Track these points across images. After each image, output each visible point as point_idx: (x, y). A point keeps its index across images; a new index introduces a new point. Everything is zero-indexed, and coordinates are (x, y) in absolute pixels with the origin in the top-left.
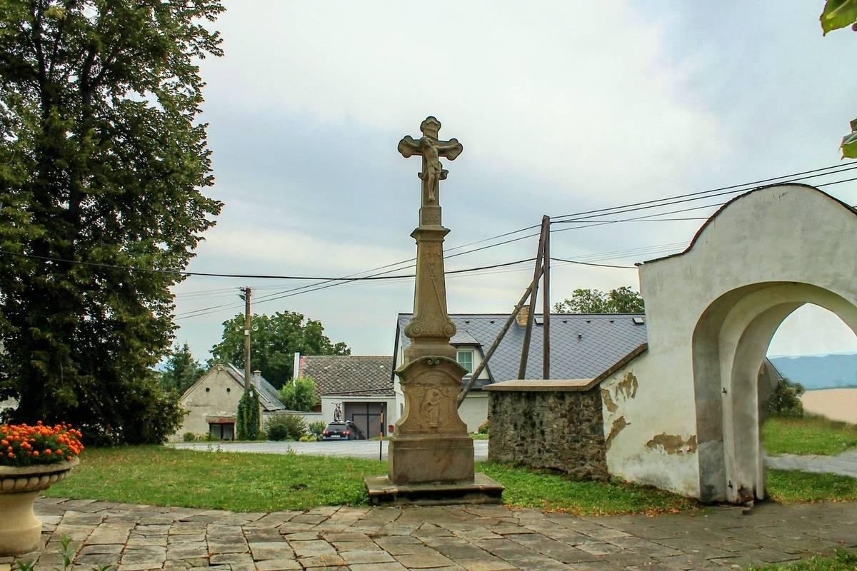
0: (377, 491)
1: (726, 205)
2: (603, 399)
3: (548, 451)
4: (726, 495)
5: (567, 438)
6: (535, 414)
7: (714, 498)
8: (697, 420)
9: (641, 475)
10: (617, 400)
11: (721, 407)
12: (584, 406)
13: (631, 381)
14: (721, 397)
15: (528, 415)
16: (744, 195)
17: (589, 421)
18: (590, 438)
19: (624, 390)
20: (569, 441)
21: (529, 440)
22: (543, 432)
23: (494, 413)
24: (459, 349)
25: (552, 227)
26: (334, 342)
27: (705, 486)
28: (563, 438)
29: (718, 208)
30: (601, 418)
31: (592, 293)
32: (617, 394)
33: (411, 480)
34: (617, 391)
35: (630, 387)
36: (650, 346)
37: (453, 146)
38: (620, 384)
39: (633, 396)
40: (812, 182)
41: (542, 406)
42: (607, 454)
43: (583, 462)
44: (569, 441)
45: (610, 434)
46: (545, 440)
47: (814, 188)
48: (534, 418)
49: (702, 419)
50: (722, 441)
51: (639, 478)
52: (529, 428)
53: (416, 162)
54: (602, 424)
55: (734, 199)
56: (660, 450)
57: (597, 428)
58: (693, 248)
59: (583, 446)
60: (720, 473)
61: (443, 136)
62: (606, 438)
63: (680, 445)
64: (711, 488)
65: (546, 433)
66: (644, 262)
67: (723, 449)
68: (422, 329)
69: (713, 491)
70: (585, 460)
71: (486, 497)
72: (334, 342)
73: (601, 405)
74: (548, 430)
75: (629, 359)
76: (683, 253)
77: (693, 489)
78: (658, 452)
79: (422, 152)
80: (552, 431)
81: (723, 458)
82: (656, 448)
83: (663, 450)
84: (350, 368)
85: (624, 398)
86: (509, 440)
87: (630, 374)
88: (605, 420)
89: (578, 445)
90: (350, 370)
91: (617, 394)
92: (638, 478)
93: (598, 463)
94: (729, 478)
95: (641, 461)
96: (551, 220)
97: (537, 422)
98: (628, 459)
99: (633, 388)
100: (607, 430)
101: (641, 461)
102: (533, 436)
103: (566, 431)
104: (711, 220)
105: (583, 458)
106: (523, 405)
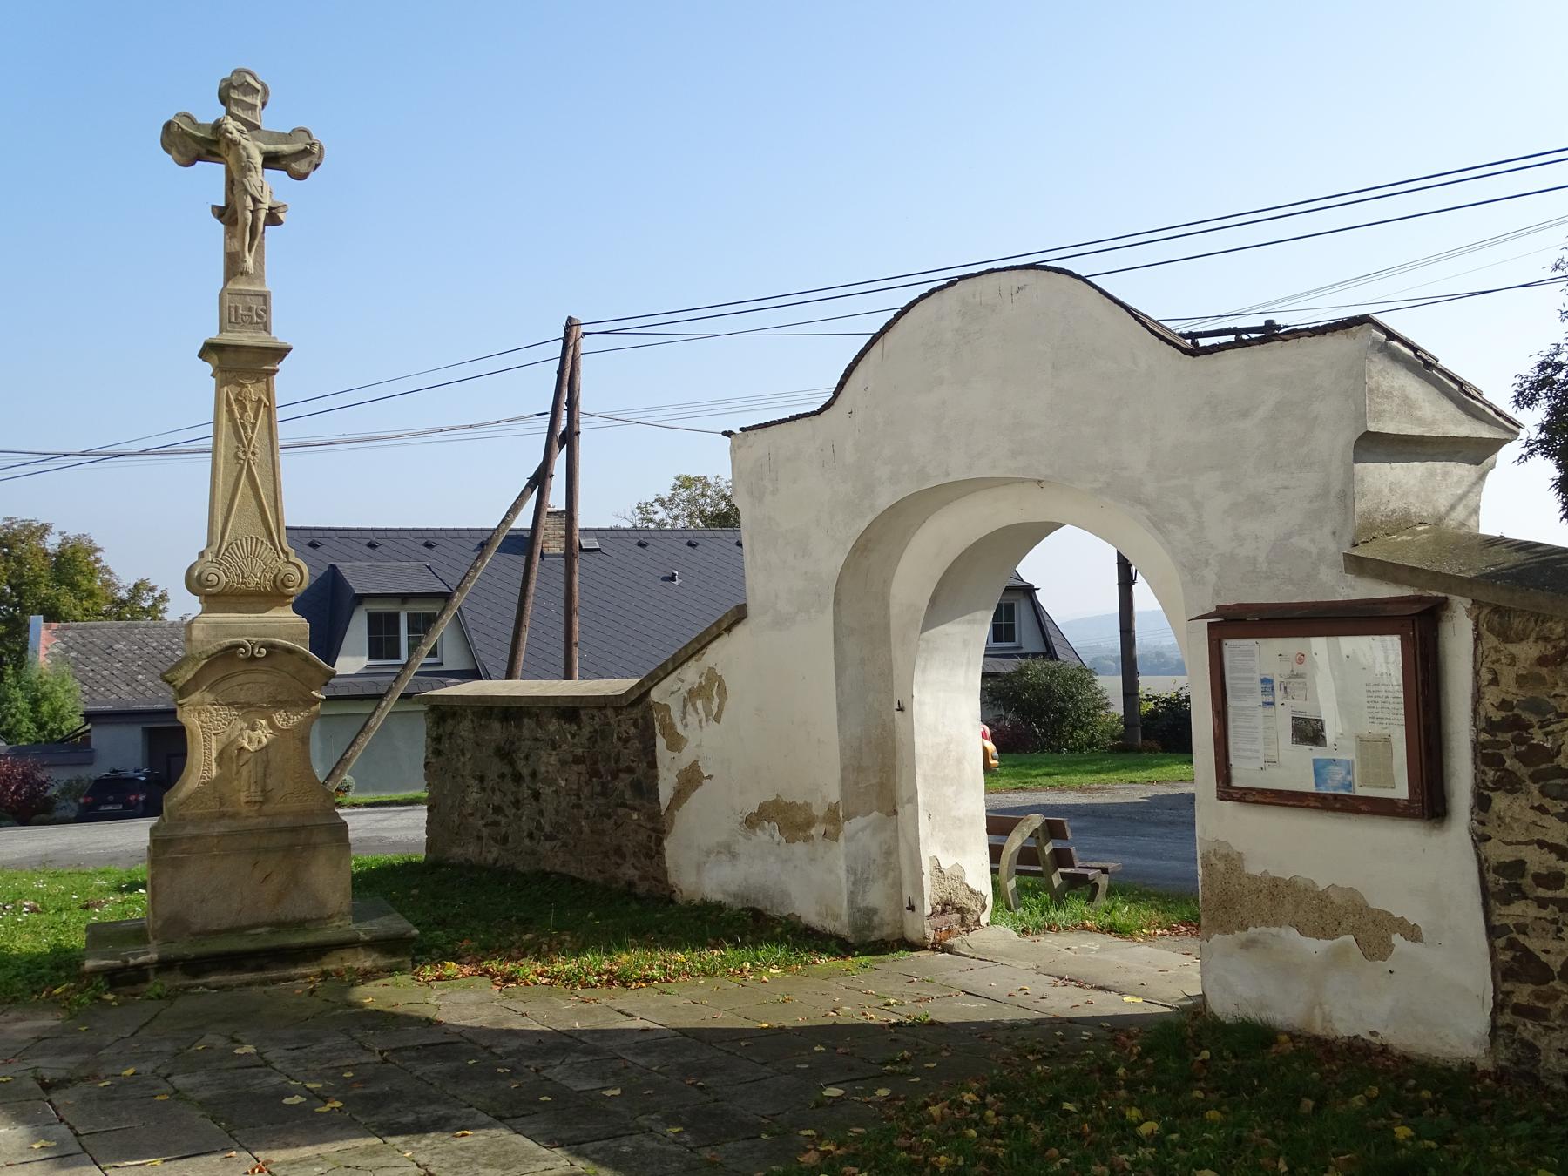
0: (111, 962)
1: (904, 311)
2: (657, 724)
3: (549, 838)
4: (902, 927)
5: (587, 808)
6: (522, 755)
7: (876, 936)
8: (843, 770)
9: (733, 888)
10: (686, 726)
11: (893, 740)
12: (619, 739)
13: (711, 689)
14: (893, 720)
15: (505, 753)
16: (940, 288)
17: (630, 770)
18: (634, 809)
19: (699, 704)
20: (591, 814)
21: (510, 811)
22: (536, 796)
23: (438, 753)
24: (407, 606)
25: (585, 345)
26: (125, 579)
27: (859, 910)
28: (578, 807)
29: (891, 315)
30: (653, 765)
31: (711, 481)
32: (684, 713)
33: (196, 928)
34: (685, 707)
35: (710, 699)
36: (751, 610)
37: (300, 146)
38: (690, 692)
39: (717, 719)
40: (1078, 266)
41: (536, 739)
42: (665, 843)
43: (619, 861)
44: (591, 814)
45: (672, 800)
46: (541, 813)
47: (1084, 279)
48: (521, 764)
49: (852, 768)
50: (896, 812)
51: (729, 895)
52: (509, 785)
53: (210, 178)
54: (656, 777)
55: (923, 297)
56: (768, 834)
57: (646, 788)
58: (836, 403)
59: (617, 825)
60: (890, 880)
61: (274, 119)
62: (664, 808)
63: (810, 823)
64: (870, 912)
65: (543, 797)
66: (742, 429)
67: (896, 830)
68: (216, 576)
69: (876, 919)
70: (624, 857)
71: (375, 956)
72: (125, 579)
73: (653, 737)
74: (547, 791)
75: (708, 638)
76: (819, 412)
77: (836, 917)
78: (767, 838)
79: (219, 156)
80: (556, 792)
81: (897, 848)
82: (763, 829)
83: (777, 834)
84: (168, 648)
85: (700, 721)
86: (471, 815)
87: (712, 670)
88: (662, 771)
89: (608, 824)
90: (168, 653)
91: (684, 713)
92: (725, 892)
93: (647, 862)
94: (907, 892)
95: (734, 856)
96: (584, 329)
97: (525, 772)
98: (708, 853)
99: (716, 701)
100: (665, 791)
101: (734, 856)
102: (517, 804)
103: (586, 791)
104: (875, 338)
105: (618, 851)
106: (497, 731)
